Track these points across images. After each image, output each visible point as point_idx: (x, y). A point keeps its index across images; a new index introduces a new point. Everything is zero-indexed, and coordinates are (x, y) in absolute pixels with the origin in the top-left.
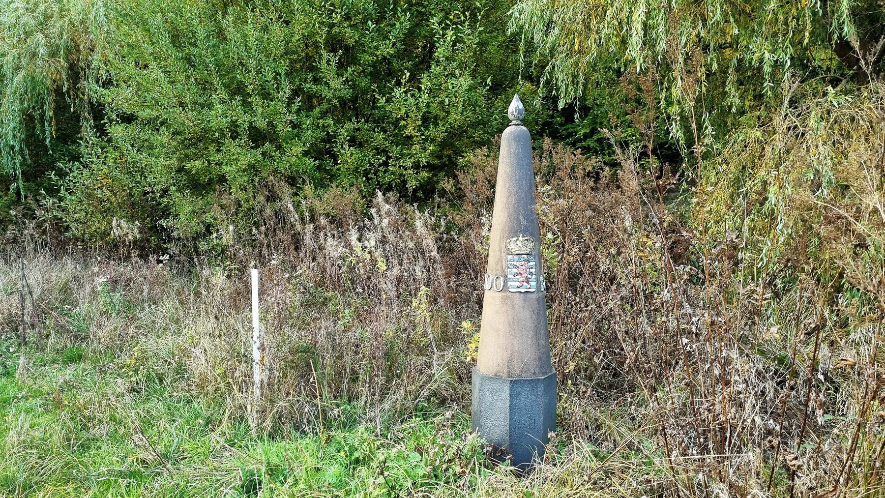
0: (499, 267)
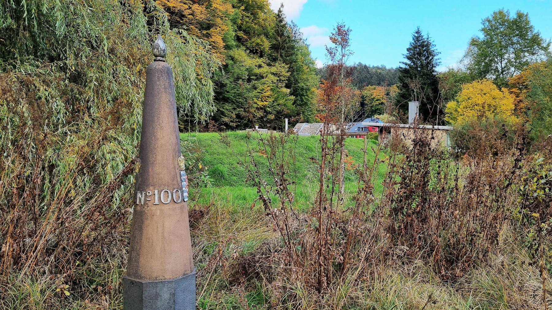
0: (175, 182)
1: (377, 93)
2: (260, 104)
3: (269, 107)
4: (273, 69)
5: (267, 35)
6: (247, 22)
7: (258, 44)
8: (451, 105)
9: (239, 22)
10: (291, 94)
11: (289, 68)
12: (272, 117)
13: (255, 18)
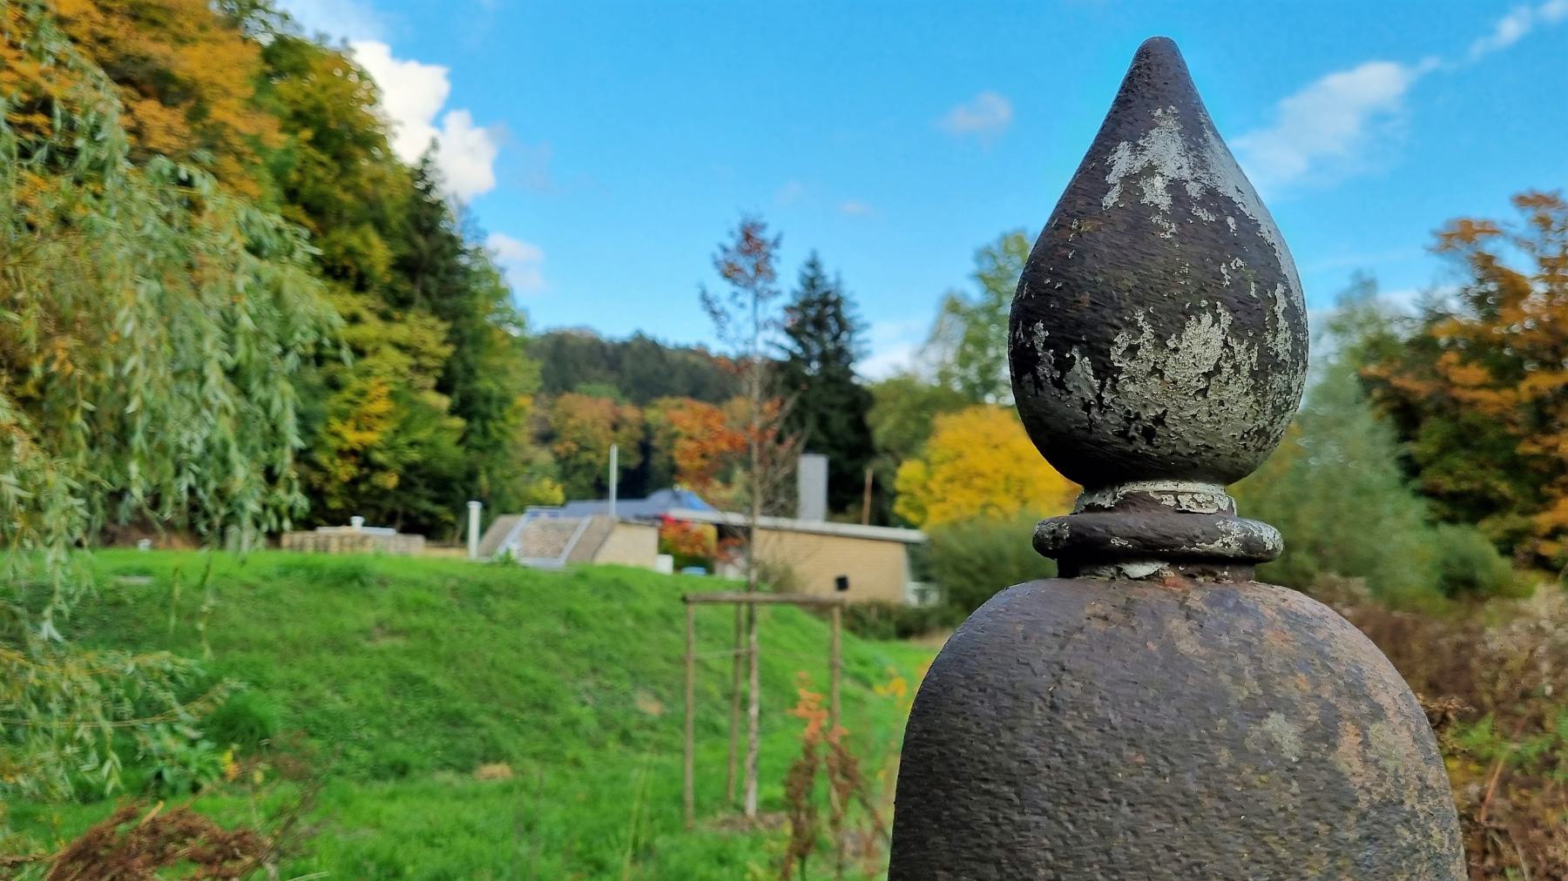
1: (678, 417)
2: (352, 437)
3: (379, 450)
4: (400, 332)
5: (380, 226)
6: (317, 180)
7: (350, 252)
8: (910, 471)
9: (294, 176)
10: (453, 412)
11: (451, 332)
12: (390, 481)
13: (345, 172)
